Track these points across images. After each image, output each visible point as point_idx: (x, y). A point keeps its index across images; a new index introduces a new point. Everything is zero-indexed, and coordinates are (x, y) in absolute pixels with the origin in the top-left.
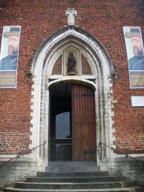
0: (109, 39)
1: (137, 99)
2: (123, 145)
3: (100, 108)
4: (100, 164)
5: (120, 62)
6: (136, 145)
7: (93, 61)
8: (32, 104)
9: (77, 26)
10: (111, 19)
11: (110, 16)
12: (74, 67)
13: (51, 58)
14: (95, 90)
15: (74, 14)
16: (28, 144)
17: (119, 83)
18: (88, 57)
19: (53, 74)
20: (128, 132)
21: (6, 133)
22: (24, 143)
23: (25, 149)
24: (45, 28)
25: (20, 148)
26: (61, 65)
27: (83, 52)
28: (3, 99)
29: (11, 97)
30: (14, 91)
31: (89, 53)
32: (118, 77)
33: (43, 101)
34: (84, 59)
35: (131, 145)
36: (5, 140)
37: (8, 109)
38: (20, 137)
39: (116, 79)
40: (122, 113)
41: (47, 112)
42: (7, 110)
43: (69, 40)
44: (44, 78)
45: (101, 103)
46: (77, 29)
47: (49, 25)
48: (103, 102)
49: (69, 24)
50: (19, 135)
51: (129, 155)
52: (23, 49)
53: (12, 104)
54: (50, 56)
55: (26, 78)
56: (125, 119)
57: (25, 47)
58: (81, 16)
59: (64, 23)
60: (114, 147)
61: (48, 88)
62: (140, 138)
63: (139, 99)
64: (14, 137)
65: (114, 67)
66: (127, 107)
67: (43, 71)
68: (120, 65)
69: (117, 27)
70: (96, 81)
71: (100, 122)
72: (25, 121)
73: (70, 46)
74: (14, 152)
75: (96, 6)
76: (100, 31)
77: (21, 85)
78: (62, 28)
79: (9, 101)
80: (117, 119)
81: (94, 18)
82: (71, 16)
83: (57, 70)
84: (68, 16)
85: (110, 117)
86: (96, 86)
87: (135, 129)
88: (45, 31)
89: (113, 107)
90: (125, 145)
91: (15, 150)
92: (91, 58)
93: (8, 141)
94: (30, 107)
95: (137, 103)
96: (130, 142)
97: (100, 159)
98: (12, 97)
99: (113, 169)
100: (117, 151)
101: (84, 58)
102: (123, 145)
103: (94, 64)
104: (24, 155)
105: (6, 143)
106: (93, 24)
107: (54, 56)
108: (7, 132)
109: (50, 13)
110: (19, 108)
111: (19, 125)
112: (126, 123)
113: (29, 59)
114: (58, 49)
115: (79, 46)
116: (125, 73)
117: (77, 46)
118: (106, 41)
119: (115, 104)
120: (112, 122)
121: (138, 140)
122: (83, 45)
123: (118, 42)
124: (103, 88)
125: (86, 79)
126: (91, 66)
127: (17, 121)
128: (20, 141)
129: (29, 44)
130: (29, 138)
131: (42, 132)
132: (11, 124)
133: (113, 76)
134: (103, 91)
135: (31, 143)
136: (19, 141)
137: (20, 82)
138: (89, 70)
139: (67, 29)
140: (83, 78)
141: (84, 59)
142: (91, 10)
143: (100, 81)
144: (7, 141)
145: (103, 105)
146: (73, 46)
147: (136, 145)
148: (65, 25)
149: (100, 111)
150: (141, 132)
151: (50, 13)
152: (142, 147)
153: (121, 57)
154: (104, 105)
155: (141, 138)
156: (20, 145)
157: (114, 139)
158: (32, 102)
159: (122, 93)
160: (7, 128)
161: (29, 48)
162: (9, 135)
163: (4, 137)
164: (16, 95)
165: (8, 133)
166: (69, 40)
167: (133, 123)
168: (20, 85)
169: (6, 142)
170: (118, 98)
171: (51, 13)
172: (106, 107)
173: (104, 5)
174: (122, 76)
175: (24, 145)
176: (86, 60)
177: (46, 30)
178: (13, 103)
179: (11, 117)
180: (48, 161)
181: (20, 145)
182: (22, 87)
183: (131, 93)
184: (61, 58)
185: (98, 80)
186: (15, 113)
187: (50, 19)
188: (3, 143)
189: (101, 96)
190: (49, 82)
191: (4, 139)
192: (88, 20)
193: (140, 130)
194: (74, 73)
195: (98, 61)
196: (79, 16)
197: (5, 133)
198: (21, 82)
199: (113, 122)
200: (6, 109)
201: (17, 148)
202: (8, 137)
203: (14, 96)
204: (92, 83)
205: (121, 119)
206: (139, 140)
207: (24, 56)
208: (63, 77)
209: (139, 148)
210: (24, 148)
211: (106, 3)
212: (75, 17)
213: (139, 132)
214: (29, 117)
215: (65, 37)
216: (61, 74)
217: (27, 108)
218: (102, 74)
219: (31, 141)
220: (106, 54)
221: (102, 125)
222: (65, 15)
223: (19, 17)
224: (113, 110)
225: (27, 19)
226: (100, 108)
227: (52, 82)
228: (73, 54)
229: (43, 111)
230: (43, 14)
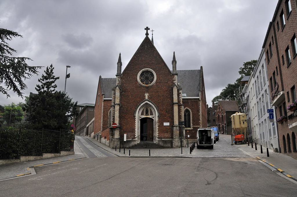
8: (135, 125)
12: (148, 113)
19: (141, 115)
41: (140, 127)
46: (148, 101)
60: (158, 137)
82: (147, 95)
83: (142, 114)
95: (158, 157)
120: (158, 130)
133: (159, 116)
139: (145, 101)
140: (150, 117)
141: (151, 110)
157: (158, 135)
204: (153, 118)
208: (143, 117)
211: (240, 106)
212: (148, 96)
220: (157, 109)
224: (158, 126)
227: (141, 118)
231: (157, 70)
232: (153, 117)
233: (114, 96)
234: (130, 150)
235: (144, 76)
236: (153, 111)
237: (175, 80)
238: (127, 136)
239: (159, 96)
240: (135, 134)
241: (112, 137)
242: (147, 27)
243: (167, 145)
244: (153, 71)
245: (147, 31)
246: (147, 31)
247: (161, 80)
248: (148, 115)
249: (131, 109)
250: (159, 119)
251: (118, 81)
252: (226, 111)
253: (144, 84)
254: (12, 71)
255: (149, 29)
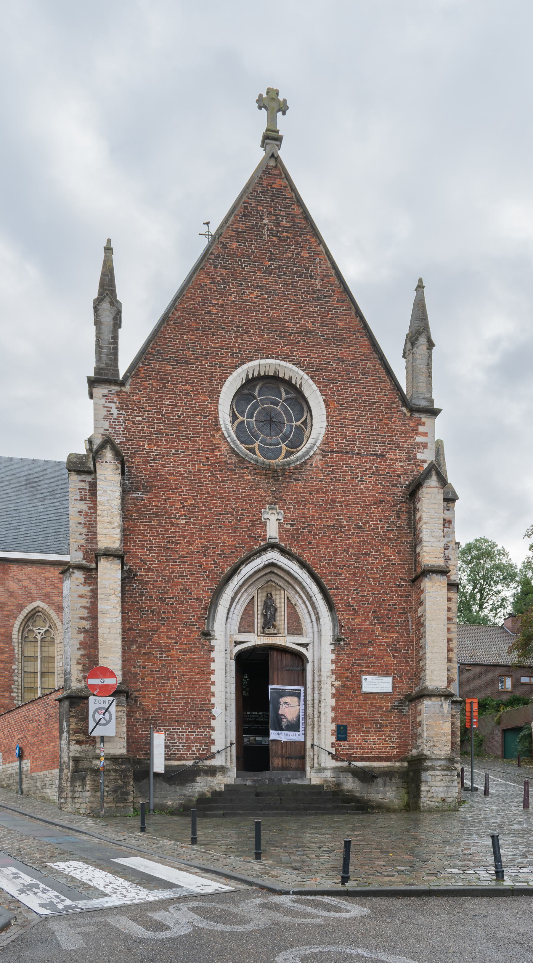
0: (335, 573)
1: (372, 681)
2: (345, 749)
3: (313, 693)
4: (311, 775)
5: (350, 617)
6: (363, 749)
7: (306, 611)
8: (213, 683)
9: (283, 545)
10: (341, 532)
11: (340, 526)
13: (237, 604)
14: (308, 662)
15: (278, 519)
16: (209, 744)
17: (345, 654)
18: (297, 603)
20: (353, 731)
21: (175, 729)
22: (203, 743)
23: (205, 752)
24: (228, 546)
25: (197, 751)
26: (254, 615)
27: (291, 593)
28: (165, 674)
29: (178, 672)
30: (182, 662)
31: (301, 597)
32: (344, 644)
33: (228, 677)
34: (291, 606)
35: (357, 749)
36: (173, 739)
37: (175, 690)
38: (198, 735)
39: (341, 647)
40: (346, 702)
41: (233, 696)
42: (173, 692)
43: (267, 571)
44: (229, 640)
45: (316, 684)
46: (284, 552)
47: (235, 539)
48: (320, 682)
49: (270, 540)
50: (195, 732)
51: (353, 763)
52: (191, 585)
53: (181, 683)
54: (237, 600)
55: (200, 639)
56: (351, 711)
57: (195, 582)
58: (290, 524)
59: (260, 537)
61: (233, 656)
62: (370, 739)
63: (373, 681)
64: (187, 735)
65: (340, 625)
66: (355, 692)
67: (226, 628)
68: (350, 623)
69: (351, 551)
70: (310, 647)
71: (313, 714)
72: (204, 710)
73: (268, 581)
74: (189, 757)
75: (318, 502)
76: (322, 557)
77: (194, 652)
78: (256, 547)
79: (176, 678)
80: (338, 710)
81: (312, 527)
84: (268, 521)
85: (509, 598)
86: (308, 654)
87: (363, 725)
88: (227, 552)
89: (334, 691)
90: (348, 749)
91: (190, 754)
92: (303, 606)
93: (179, 740)
94: (209, 688)
96: (356, 744)
97: (311, 768)
98: (180, 672)
99: (330, 782)
100: (335, 757)
101: (292, 604)
102: (345, 749)
103: (307, 616)
104: (205, 761)
105: (176, 743)
106: (310, 543)
107: (242, 599)
108: (176, 726)
109: (234, 513)
110: (192, 690)
111: (194, 716)
112: (351, 717)
113: (204, 605)
114: (249, 586)
115: (284, 581)
116: (356, 636)
117: (280, 581)
118: (330, 577)
119: (337, 689)
121: (367, 741)
122: (291, 582)
123: (350, 580)
124: (320, 660)
125: (294, 643)
126: (302, 621)
127: (190, 710)
128: (197, 740)
129: (201, 577)
130: (211, 735)
131: (228, 728)
132: (182, 715)
133: (337, 640)
134: (320, 665)
135: (214, 744)
136: (196, 741)
137: (191, 647)
138: (298, 626)
139: (264, 550)
141: (290, 606)
142: (308, 509)
143: (316, 648)
144: (177, 739)
145: (318, 688)
146: (273, 582)
147: (363, 749)
148: (262, 540)
149: (314, 697)
150: (372, 731)
151: (234, 513)
152: (371, 752)
153: (353, 609)
154: (320, 689)
155: (371, 740)
156: (198, 746)
158: (212, 680)
159: (348, 670)
160: (176, 721)
161: (202, 586)
162: (180, 732)
163: (172, 735)
164: (186, 669)
165: (178, 729)
166: (267, 571)
167: (362, 717)
168: (192, 652)
169: (175, 741)
170: (343, 678)
171: (237, 513)
172: (323, 691)
173: (333, 501)
174: (351, 641)
175: (203, 747)
176: (294, 607)
177: (229, 549)
178: (183, 681)
179: (181, 703)
180: (238, 769)
181: (198, 746)
182: (194, 655)
183: (363, 671)
184: (254, 602)
185: (313, 646)
186: (186, 698)
187: (235, 527)
188: (172, 743)
189: (316, 674)
190: (235, 646)
191: (172, 738)
192: (302, 532)
193: (371, 728)
194: (275, 632)
195: (314, 613)
196: (287, 524)
197: (173, 729)
198: (193, 647)
199: (333, 715)
200: (171, 690)
201: (194, 751)
202: (179, 735)
203: (183, 669)
204: (302, 650)
205: (344, 711)
206: (369, 742)
207: (194, 599)
209: (367, 753)
210: (203, 751)
213: (369, 731)
214: (209, 704)
215: (261, 566)
216: (254, 632)
217: (206, 690)
218: (320, 636)
219: (214, 740)
221: (316, 719)
222: (261, 519)
223: (179, 519)
225: (194, 524)
226: (313, 693)
227: (240, 647)
228: (273, 595)
229: (228, 695)
230: (223, 514)
231: (331, 380)
232: (305, 645)
233: (83, 506)
234: (258, 824)
235: (255, 407)
236: (302, 610)
237: (425, 445)
238: (167, 747)
239: (337, 528)
240: (214, 736)
241: (78, 747)
242: (273, 94)
243: (380, 796)
244: (306, 377)
245: (272, 120)
246: (272, 120)
247: (353, 439)
248: (252, 632)
249: (185, 591)
250: (338, 656)
251: (105, 418)
252: (462, 664)
253: (252, 451)
254: (293, 207)
255: (283, 108)
